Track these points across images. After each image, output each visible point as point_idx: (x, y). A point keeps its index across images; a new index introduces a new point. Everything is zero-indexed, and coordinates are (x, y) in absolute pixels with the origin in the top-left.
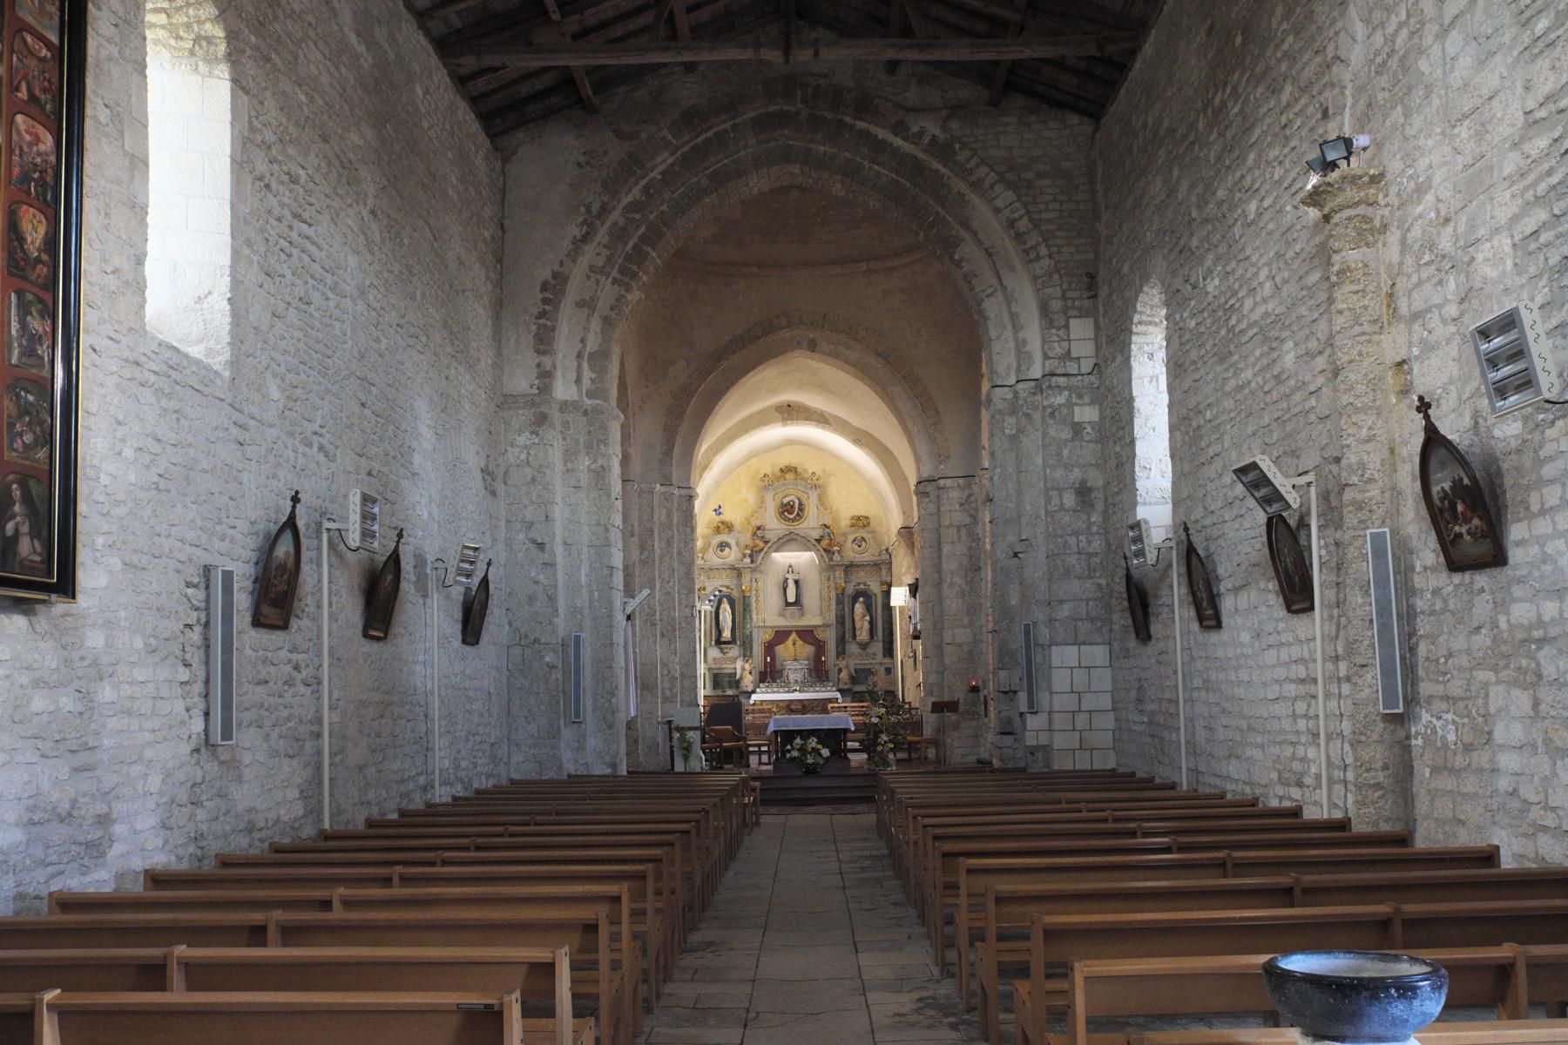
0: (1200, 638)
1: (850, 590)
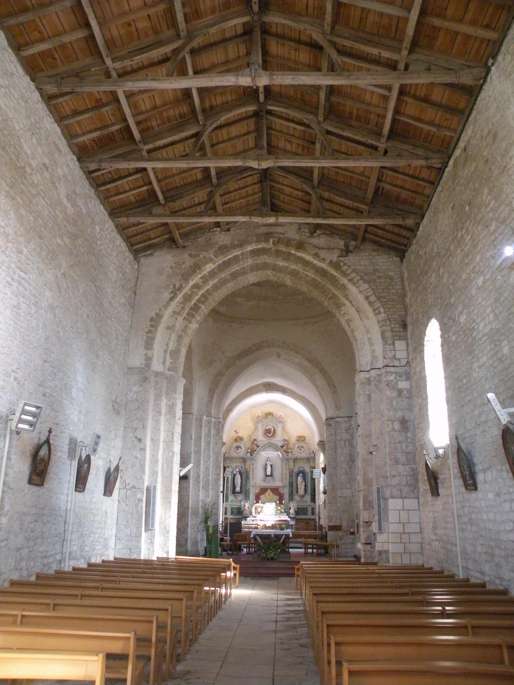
0: (466, 496)
1: (296, 470)
